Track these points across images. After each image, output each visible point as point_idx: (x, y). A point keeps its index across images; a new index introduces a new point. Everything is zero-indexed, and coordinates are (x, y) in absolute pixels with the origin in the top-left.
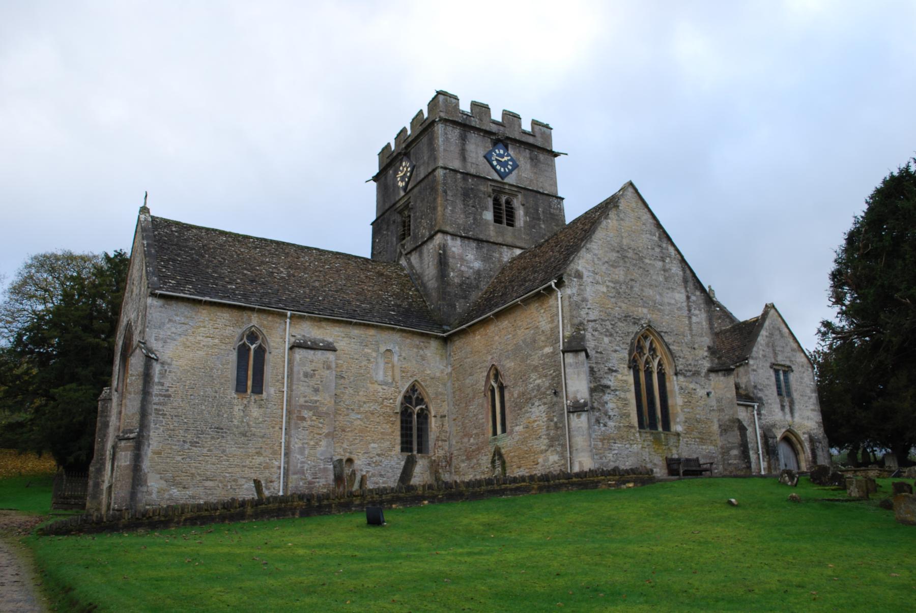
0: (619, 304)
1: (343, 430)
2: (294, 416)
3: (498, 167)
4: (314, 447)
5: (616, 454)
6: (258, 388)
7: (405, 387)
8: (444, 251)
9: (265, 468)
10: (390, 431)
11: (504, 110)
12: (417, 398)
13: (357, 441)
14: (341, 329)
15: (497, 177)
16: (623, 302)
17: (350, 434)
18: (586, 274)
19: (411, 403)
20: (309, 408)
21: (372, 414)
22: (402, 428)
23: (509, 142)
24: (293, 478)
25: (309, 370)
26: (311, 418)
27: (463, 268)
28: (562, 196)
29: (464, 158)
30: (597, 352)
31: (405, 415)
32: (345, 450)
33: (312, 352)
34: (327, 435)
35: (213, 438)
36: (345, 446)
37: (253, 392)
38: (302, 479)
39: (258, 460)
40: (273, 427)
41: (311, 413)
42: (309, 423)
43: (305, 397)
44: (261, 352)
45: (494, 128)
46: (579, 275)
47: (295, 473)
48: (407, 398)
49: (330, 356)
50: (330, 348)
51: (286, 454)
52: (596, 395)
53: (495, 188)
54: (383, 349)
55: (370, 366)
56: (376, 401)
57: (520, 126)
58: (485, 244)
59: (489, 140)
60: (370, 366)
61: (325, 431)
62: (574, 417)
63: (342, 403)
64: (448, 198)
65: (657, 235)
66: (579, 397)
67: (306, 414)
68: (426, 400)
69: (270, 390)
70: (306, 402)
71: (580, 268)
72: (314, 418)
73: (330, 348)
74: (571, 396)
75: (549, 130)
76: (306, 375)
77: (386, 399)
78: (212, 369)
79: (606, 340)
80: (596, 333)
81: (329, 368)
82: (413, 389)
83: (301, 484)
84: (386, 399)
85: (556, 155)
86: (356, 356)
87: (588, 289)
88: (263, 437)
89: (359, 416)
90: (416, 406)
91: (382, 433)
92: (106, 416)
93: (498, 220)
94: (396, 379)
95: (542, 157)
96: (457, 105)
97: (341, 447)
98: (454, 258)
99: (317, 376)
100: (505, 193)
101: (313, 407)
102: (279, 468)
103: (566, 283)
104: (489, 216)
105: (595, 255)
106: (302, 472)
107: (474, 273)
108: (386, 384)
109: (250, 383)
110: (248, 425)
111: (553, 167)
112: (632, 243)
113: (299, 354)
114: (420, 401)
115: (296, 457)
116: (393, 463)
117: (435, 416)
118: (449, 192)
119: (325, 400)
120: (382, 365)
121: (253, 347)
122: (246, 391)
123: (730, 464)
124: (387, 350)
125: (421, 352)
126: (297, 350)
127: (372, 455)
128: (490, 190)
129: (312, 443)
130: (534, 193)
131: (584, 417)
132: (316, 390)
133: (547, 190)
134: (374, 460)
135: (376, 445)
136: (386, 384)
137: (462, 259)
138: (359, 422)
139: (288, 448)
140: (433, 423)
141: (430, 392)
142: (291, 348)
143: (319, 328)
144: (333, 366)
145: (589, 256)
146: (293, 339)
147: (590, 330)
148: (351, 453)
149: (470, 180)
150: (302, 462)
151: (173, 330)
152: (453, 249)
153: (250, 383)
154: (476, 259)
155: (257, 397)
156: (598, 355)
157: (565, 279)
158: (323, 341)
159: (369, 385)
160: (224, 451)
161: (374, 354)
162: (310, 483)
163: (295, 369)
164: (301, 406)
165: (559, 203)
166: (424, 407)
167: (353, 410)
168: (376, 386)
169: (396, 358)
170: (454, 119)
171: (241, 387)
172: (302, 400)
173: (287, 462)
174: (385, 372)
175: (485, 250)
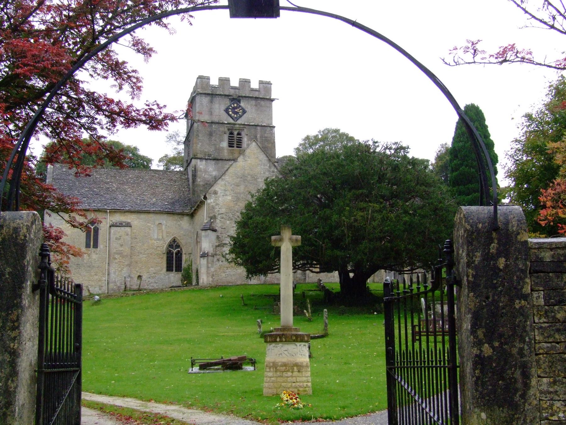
0: (239, 204)
1: (136, 263)
2: (111, 258)
3: (233, 115)
4: (121, 271)
5: (228, 274)
6: (96, 246)
7: (169, 240)
8: (195, 169)
9: (99, 281)
10: (160, 262)
11: (240, 79)
12: (176, 245)
13: (143, 267)
14: (135, 215)
15: (231, 121)
16: (241, 203)
17: (140, 264)
18: (219, 191)
19: (172, 248)
20: (118, 254)
21: (151, 254)
22: (167, 260)
23: (241, 98)
24: (111, 285)
25: (118, 237)
26: (119, 258)
27: (206, 176)
28: (275, 125)
29: (211, 113)
30: (222, 228)
31: (169, 255)
32: (137, 271)
33: (120, 228)
34: (127, 265)
35: (75, 269)
36: (137, 270)
37: (93, 247)
38: (115, 285)
39: (97, 277)
40: (103, 263)
41: (119, 256)
42: (118, 260)
43: (116, 249)
44: (96, 231)
45: (232, 92)
46: (215, 193)
47: (111, 283)
48: (170, 246)
49: (128, 229)
50: (128, 225)
51: (108, 275)
52: (219, 248)
53: (229, 128)
54: (157, 223)
55: (150, 232)
56: (153, 248)
57: (250, 86)
58: (220, 161)
59: (228, 99)
60: (150, 232)
61: (126, 263)
62: (202, 259)
63: (136, 250)
64: (199, 138)
65: (268, 165)
66: (206, 250)
67: (117, 256)
68: (181, 246)
69: (101, 246)
70: (117, 251)
71: (217, 189)
72: (121, 258)
73: (128, 225)
74: (203, 249)
75: (270, 85)
76: (116, 239)
77: (159, 247)
78: (74, 239)
79: (228, 222)
80: (222, 220)
81: (127, 235)
82: (174, 240)
83: (115, 287)
84: (159, 247)
85: (272, 100)
86: (143, 228)
87: (220, 199)
88: (98, 267)
89: (145, 256)
90: (175, 249)
91: (156, 263)
92: (541, 112)
93: (231, 145)
94: (164, 237)
95: (263, 103)
96: (209, 82)
97: (135, 270)
98: (201, 171)
99: (122, 239)
100: (236, 129)
101: (120, 253)
102: (105, 281)
103: (208, 197)
104: (225, 144)
105: (227, 181)
106: (115, 282)
107: (212, 178)
108: (158, 239)
109: (92, 243)
110: (91, 262)
111: (270, 107)
112: (251, 172)
113: (113, 229)
114: (178, 246)
115: (112, 275)
116: (162, 277)
117: (185, 254)
118: (200, 135)
119: (126, 250)
120: (156, 231)
121: (92, 228)
122: (90, 247)
123: (297, 277)
124: (159, 223)
125: (179, 223)
126: (112, 228)
127: (150, 273)
128: (226, 129)
129: (120, 269)
130: (254, 127)
131: (206, 259)
132: (122, 245)
133: (265, 123)
134: (152, 275)
135: (153, 269)
136: (158, 239)
137: (206, 171)
138: (144, 259)
139: (109, 272)
140: (184, 257)
141: (182, 242)
142: (110, 226)
143: (124, 216)
144: (130, 233)
145: (223, 183)
146: (111, 222)
147: (219, 218)
148: (140, 273)
149: (213, 126)
150: (115, 278)
151: (56, 223)
152: (201, 167)
153: (92, 243)
154: (214, 170)
155: (94, 249)
156: (222, 230)
157: (207, 196)
158: (125, 222)
159: (150, 241)
160: (80, 274)
161: (152, 226)
162: (119, 287)
163: (112, 236)
164: (115, 253)
165: (272, 130)
166: (179, 249)
167: (141, 253)
168: (153, 241)
169: (164, 227)
170: (206, 92)
171: (88, 246)
172: (115, 251)
173: (108, 278)
174: (158, 234)
175: (220, 165)
